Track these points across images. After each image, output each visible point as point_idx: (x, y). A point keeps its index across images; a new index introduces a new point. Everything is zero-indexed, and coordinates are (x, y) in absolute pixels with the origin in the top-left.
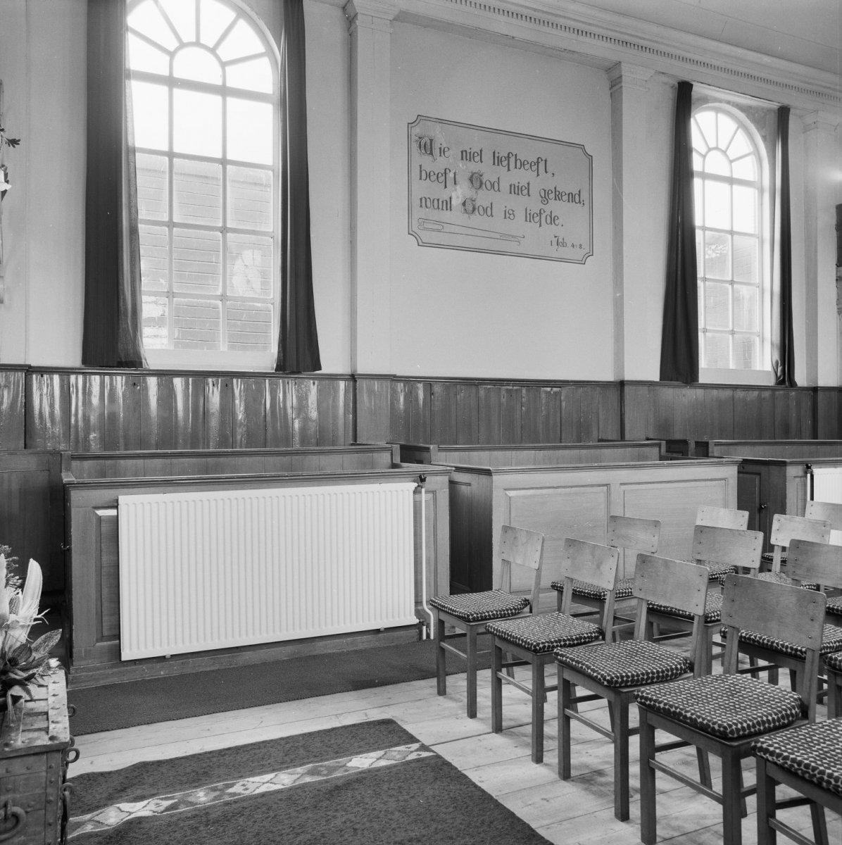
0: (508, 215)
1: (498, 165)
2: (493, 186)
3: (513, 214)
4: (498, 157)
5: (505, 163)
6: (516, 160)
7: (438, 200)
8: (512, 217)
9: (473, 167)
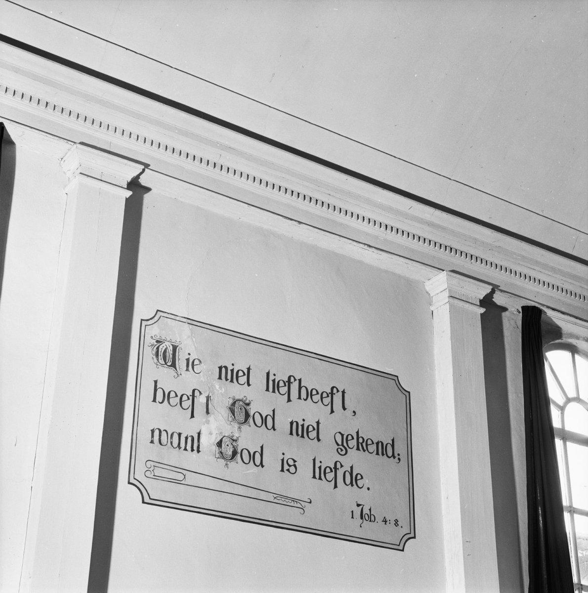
0: (286, 467)
1: (274, 391)
2: (252, 457)
3: (295, 466)
4: (274, 381)
5: (284, 390)
6: (300, 388)
7: (180, 435)
8: (292, 469)
9: (238, 391)
